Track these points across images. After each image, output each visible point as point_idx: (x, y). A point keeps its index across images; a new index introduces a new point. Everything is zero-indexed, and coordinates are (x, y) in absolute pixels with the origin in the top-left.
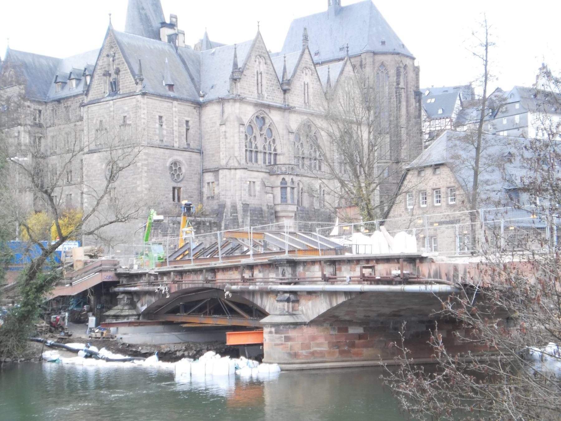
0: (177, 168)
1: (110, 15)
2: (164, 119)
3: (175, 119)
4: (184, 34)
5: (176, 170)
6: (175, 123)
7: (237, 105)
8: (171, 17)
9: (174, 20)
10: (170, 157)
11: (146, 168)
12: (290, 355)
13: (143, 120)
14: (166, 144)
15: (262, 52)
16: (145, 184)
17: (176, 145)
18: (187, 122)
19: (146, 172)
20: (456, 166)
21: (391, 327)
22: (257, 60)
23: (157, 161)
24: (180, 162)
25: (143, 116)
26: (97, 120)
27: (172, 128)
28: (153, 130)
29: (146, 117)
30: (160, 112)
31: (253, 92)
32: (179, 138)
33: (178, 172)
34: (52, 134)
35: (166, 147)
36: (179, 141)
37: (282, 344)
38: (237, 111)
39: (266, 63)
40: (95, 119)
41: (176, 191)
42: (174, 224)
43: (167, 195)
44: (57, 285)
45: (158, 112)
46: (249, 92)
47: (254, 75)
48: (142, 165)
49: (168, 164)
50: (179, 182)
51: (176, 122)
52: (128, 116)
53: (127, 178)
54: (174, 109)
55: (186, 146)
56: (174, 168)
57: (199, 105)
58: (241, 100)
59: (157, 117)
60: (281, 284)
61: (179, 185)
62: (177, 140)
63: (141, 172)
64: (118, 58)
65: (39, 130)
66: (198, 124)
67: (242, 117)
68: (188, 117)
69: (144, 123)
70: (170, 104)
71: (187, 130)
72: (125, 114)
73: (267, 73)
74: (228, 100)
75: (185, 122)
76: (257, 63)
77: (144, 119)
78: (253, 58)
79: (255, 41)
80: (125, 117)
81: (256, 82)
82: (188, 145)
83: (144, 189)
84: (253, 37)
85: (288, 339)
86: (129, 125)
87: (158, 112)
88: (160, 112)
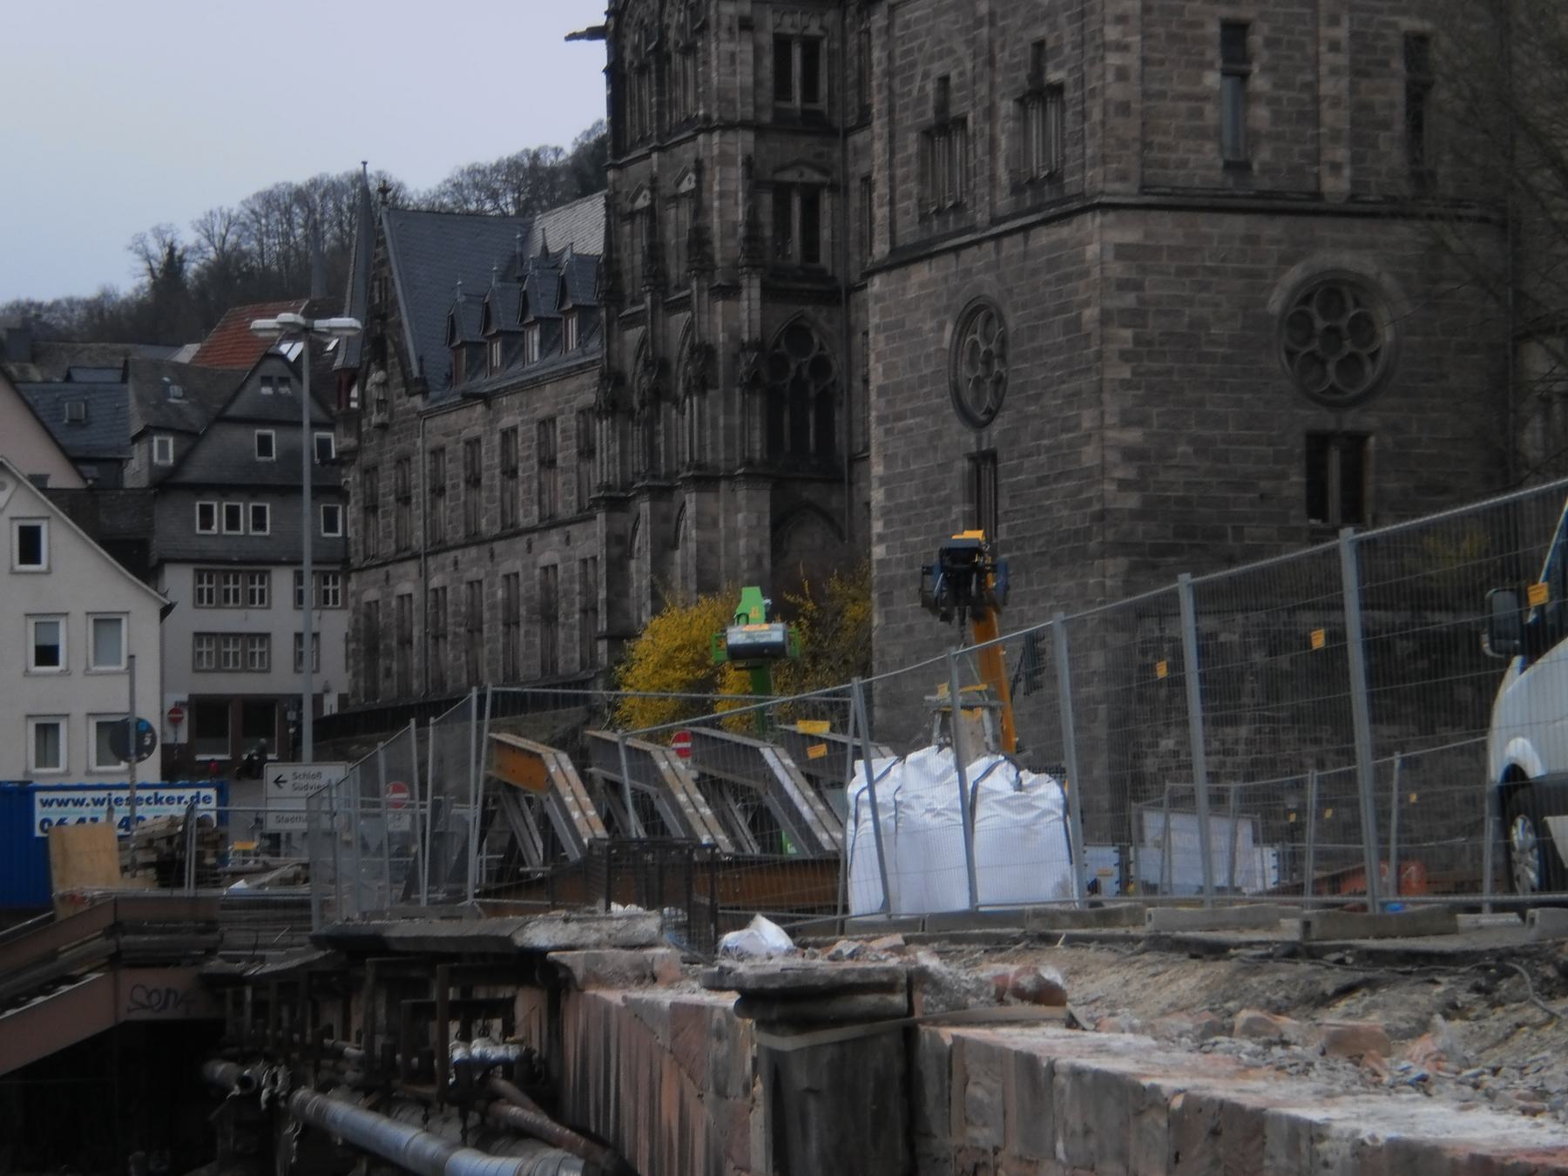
0: (1343, 323)
2: (1256, 40)
3: (1327, 32)
5: (1332, 331)
6: (1328, 58)
10: (1287, 261)
11: (1127, 334)
13: (1113, 59)
14: (1266, 184)
16: (1126, 422)
17: (1336, 185)
19: (1125, 356)
20: (262, 255)
23: (1205, 287)
24: (1361, 286)
25: (1112, 33)
26: (926, 76)
27: (1311, 87)
28: (1183, 106)
33: (1348, 347)
35: (1269, 205)
36: (1356, 159)
40: (920, 70)
41: (1334, 459)
42: (1273, 652)
43: (1265, 485)
44: (1110, 949)
48: (1106, 318)
49: (1276, 303)
50: (1356, 401)
51: (1334, 47)
52: (1050, 44)
53: (1037, 398)
55: (1405, 189)
56: (1320, 324)
59: (1213, 29)
61: (1351, 421)
62: (1341, 154)
63: (1100, 355)
65: (805, 146)
69: (1122, 74)
71: (1417, 95)
72: (1040, 32)
77: (1123, 48)
80: (1039, 45)
83: (1113, 456)
86: (1058, 89)
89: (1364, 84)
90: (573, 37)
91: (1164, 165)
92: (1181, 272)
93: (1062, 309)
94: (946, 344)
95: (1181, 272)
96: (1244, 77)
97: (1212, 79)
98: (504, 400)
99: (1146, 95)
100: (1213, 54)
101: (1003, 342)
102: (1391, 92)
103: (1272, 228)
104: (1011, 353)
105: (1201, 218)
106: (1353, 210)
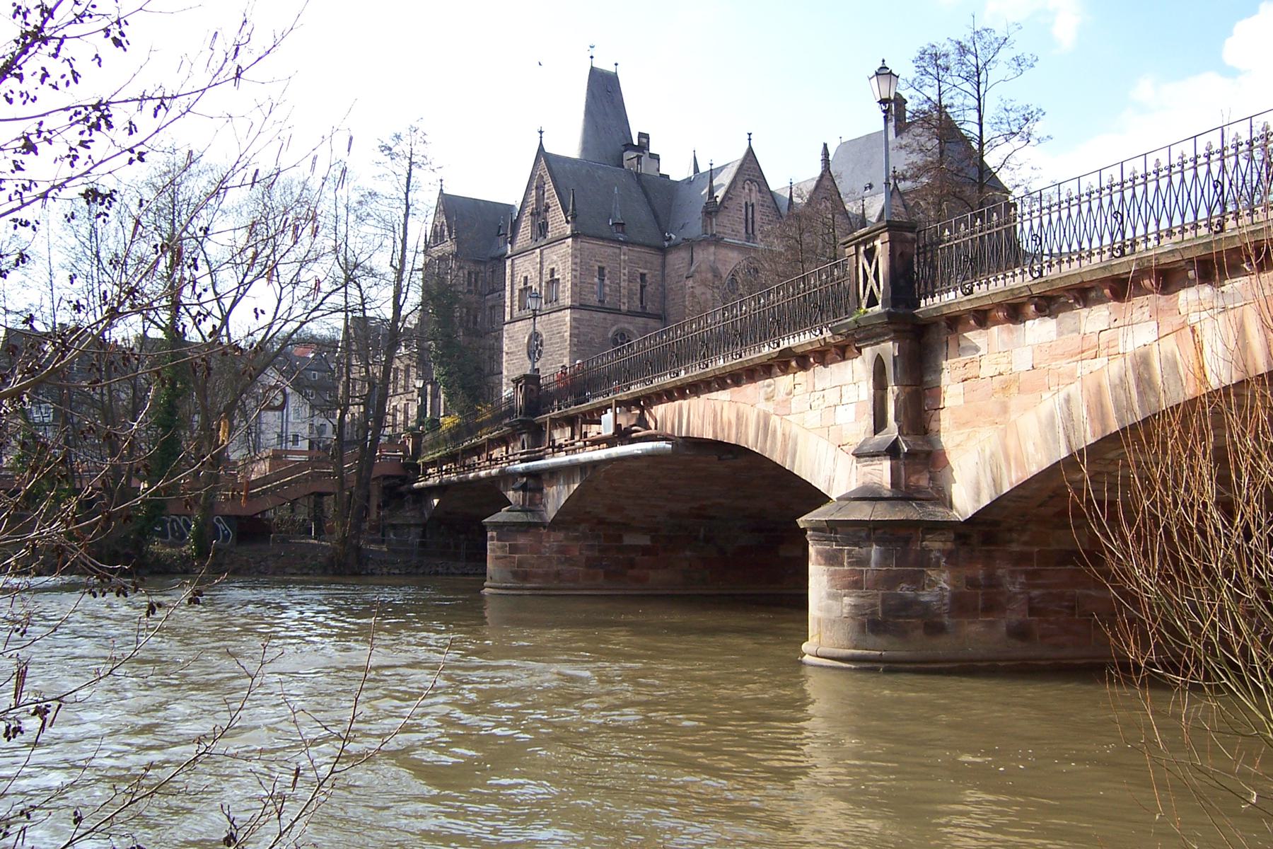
1: (541, 132)
2: (606, 271)
4: (659, 160)
6: (623, 277)
7: (712, 249)
8: (641, 135)
9: (644, 140)
11: (576, 340)
12: (515, 574)
15: (754, 176)
17: (624, 308)
18: (643, 276)
21: (701, 536)
22: (746, 186)
23: (594, 330)
24: (629, 331)
27: (619, 284)
29: (578, 269)
30: (601, 262)
31: (738, 232)
32: (630, 298)
34: (490, 304)
37: (505, 557)
38: (712, 258)
39: (760, 191)
45: (597, 261)
46: (733, 231)
47: (741, 207)
49: (610, 335)
51: (624, 275)
54: (622, 257)
57: (663, 251)
58: (717, 241)
60: (522, 461)
62: (626, 300)
64: (548, 191)
66: (659, 279)
67: (719, 266)
68: (645, 269)
70: (618, 251)
71: (642, 287)
73: (762, 205)
74: (699, 243)
75: (639, 275)
76: (747, 191)
78: (740, 184)
79: (822, 176)
80: (553, 269)
81: (744, 217)
82: (644, 308)
84: (740, 154)
85: (514, 549)
86: (558, 279)
87: (597, 261)
88: (601, 262)
89: (631, 284)
90: (825, 145)
91: (584, 299)
92: (588, 326)
93: (559, 333)
94: (526, 342)
95: (588, 326)
96: (603, 280)
97: (596, 280)
98: (660, 261)
99: (581, 282)
100: (596, 274)
101: (542, 341)
102: (637, 287)
103: (610, 317)
104: (544, 344)
105: (593, 313)
106: (630, 313)
